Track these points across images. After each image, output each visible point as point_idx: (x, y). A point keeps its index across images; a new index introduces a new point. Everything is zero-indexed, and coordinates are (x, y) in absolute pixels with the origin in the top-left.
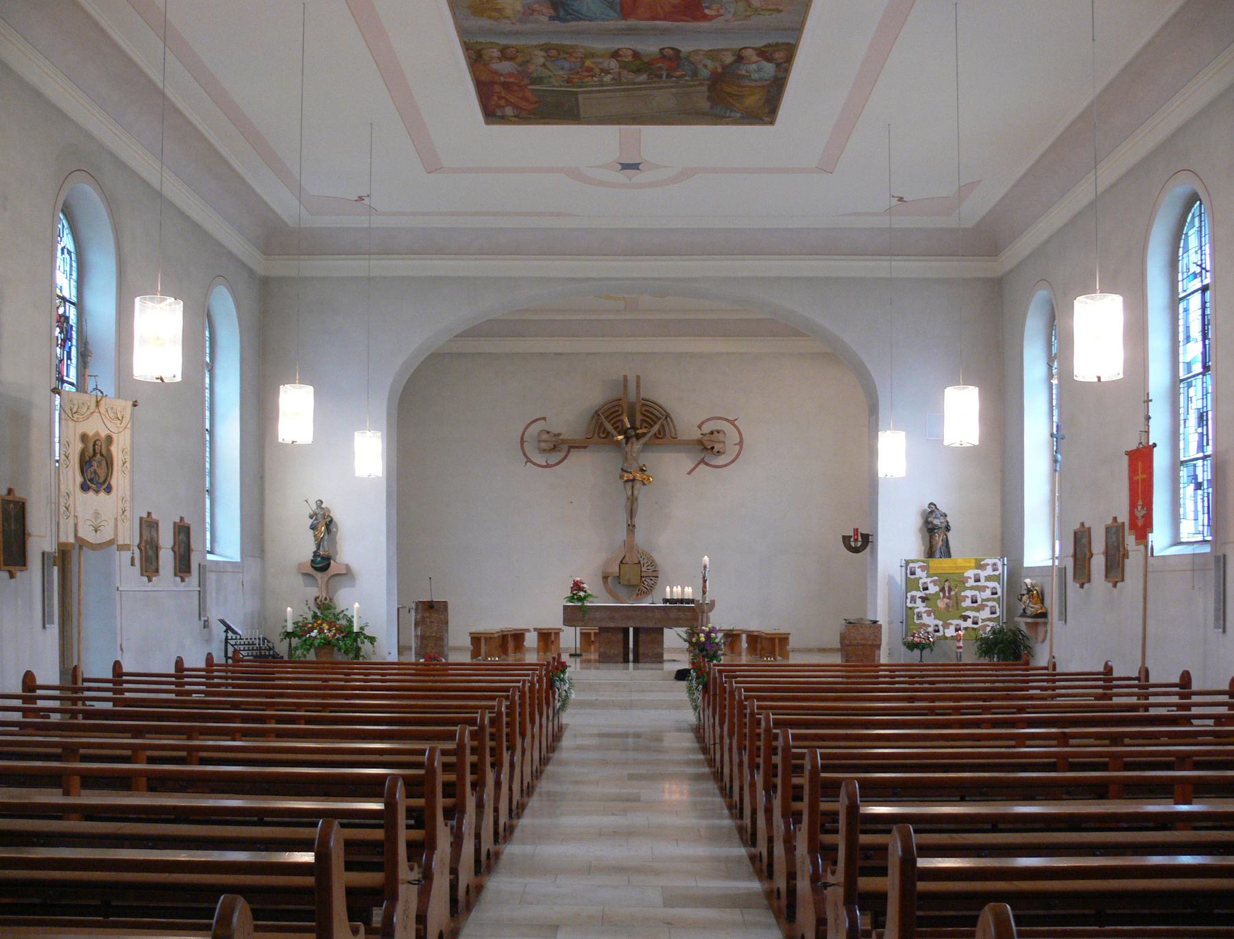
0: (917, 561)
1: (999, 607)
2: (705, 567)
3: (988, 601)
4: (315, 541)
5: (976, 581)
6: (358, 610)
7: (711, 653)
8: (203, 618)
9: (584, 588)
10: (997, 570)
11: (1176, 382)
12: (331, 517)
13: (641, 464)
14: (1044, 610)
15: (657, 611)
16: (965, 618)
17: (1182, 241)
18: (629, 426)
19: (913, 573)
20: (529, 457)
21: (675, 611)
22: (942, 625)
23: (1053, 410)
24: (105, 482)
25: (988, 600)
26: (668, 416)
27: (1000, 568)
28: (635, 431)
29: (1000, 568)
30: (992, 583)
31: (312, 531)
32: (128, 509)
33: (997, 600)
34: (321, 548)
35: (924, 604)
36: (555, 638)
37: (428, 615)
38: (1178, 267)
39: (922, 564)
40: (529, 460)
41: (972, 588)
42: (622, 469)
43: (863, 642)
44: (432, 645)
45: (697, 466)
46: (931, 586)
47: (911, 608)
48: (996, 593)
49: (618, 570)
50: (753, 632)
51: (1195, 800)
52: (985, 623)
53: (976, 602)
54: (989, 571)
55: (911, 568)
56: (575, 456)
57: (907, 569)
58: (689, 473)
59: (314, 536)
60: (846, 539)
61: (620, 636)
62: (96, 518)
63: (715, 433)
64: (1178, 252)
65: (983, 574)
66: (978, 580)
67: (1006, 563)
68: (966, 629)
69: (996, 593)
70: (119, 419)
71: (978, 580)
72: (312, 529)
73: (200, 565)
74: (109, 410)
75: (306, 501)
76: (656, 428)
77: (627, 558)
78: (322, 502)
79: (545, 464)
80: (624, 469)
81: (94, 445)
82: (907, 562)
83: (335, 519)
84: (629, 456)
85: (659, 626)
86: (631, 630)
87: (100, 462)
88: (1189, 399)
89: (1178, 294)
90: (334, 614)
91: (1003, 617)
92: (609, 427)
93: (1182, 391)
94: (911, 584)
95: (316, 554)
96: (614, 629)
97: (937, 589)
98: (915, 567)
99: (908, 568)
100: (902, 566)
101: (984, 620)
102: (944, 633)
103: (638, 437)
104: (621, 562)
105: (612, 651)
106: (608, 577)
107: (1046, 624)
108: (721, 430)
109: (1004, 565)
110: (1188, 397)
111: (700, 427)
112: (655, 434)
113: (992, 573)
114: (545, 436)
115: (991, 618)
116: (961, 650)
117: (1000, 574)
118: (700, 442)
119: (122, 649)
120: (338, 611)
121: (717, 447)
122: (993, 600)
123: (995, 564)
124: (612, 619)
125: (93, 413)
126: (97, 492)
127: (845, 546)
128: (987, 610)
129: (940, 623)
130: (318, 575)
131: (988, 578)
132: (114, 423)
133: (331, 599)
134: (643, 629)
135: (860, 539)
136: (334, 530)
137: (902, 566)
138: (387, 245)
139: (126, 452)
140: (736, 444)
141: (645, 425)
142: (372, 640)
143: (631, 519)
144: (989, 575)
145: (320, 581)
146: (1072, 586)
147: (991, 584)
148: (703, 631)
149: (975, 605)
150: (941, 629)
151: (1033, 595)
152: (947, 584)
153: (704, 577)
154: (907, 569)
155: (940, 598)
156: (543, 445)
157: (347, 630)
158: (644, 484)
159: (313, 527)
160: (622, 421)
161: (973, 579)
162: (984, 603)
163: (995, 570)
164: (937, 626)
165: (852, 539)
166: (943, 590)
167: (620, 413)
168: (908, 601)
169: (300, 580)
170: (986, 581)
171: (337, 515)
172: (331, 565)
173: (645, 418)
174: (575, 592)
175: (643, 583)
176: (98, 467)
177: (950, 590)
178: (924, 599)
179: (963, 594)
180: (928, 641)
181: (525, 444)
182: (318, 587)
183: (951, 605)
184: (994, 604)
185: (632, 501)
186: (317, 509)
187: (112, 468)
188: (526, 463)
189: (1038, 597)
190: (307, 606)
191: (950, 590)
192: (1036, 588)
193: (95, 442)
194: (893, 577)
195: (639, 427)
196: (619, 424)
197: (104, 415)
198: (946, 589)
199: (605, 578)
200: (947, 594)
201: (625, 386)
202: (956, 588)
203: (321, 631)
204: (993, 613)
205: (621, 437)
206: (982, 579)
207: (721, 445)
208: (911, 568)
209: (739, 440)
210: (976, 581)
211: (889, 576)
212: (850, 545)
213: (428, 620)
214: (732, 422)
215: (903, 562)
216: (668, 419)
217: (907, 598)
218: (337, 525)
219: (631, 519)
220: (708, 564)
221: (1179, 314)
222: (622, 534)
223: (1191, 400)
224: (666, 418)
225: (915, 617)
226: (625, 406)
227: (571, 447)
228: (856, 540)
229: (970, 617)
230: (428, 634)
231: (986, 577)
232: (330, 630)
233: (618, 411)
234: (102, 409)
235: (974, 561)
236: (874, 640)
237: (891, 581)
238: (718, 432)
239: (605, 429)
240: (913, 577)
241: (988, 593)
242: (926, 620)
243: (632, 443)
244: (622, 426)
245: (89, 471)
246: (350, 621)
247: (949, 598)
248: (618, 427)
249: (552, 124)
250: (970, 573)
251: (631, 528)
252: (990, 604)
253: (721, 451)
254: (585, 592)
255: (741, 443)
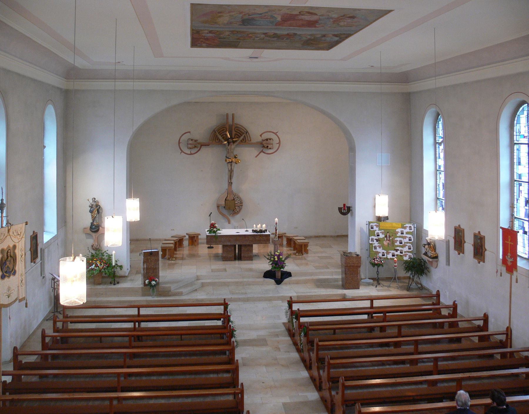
0: (374, 223)
1: (412, 246)
2: (276, 224)
3: (407, 243)
4: (92, 218)
5: (401, 234)
6: (115, 254)
7: (281, 266)
8: (43, 276)
9: (216, 226)
10: (412, 229)
11: (512, 181)
12: (99, 206)
13: (235, 154)
14: (436, 255)
15: (250, 237)
16: (397, 250)
17: (516, 118)
18: (230, 137)
19: (372, 228)
20: (183, 150)
21: (259, 237)
22: (386, 253)
23: (436, 159)
24: (13, 270)
25: (407, 243)
26: (247, 132)
27: (413, 228)
28: (232, 140)
29: (413, 228)
30: (409, 235)
31: (90, 213)
32: (24, 279)
33: (412, 243)
34: (95, 221)
35: (378, 243)
36: (197, 238)
37: (150, 258)
38: (514, 129)
39: (376, 224)
40: (182, 151)
41: (400, 237)
42: (226, 157)
43: (353, 265)
44: (152, 272)
45: (260, 153)
46: (380, 234)
47: (371, 244)
48: (411, 240)
49: (224, 203)
50: (290, 237)
51: (520, 368)
52: (406, 253)
53: (402, 243)
54: (408, 230)
55: (371, 226)
56: (204, 149)
57: (369, 226)
58: (256, 157)
59: (92, 216)
60: (340, 209)
61: (233, 248)
62: (9, 290)
63: (269, 140)
64: (514, 122)
65: (405, 231)
66: (402, 233)
67: (415, 227)
68: (397, 255)
69: (411, 240)
70: (19, 235)
71: (402, 233)
72: (91, 212)
73: (41, 249)
74: (14, 232)
75: (88, 200)
76: (242, 138)
77: (228, 197)
78: (95, 199)
79: (190, 153)
80: (227, 156)
81: (7, 253)
82: (369, 223)
83: (101, 206)
84: (229, 151)
85: (251, 244)
86: (237, 246)
87: (10, 261)
88: (520, 191)
89: (514, 141)
90: (101, 253)
91: (414, 251)
92: (220, 137)
93: (515, 185)
94: (371, 232)
95: (92, 224)
96: (231, 246)
97: (383, 236)
98: (373, 225)
99: (370, 225)
100: (367, 224)
101: (405, 252)
102: (387, 256)
103: (234, 142)
104: (226, 200)
105: (229, 255)
106: (219, 206)
107: (437, 261)
108: (272, 139)
109: (414, 227)
110: (519, 190)
111: (261, 136)
112: (241, 140)
113: (409, 231)
114: (190, 142)
115: (409, 251)
116: (396, 267)
117: (413, 231)
118: (262, 143)
119: (10, 318)
120: (103, 251)
121: (270, 146)
122: (410, 243)
123: (410, 227)
124: (229, 241)
125: (7, 236)
126: (9, 277)
127: (339, 212)
128: (407, 247)
129: (385, 252)
130: (94, 234)
131: (407, 233)
132: (17, 238)
133: (99, 245)
134: (244, 245)
135: (346, 209)
136: (101, 211)
137: (367, 224)
138: (127, 76)
139: (23, 250)
140: (277, 144)
141: (236, 136)
142: (121, 267)
143: (230, 179)
144: (408, 232)
145: (94, 237)
146: (453, 253)
147: (409, 236)
148: (276, 255)
149: (401, 245)
150: (385, 254)
151: (431, 247)
152: (388, 234)
153: (276, 228)
154: (369, 226)
155: (385, 240)
156: (190, 146)
157: (109, 263)
158: (236, 163)
159: (91, 212)
160: (226, 135)
161: (400, 233)
162: (405, 244)
163: (410, 229)
164: (383, 253)
165: (343, 209)
166: (386, 236)
167: (225, 131)
168: (370, 240)
169: (84, 236)
170: (406, 234)
171: (102, 204)
172: (100, 229)
173: (237, 133)
174: (212, 229)
175: (236, 209)
176: (9, 264)
177: (390, 237)
178: (377, 240)
179: (395, 239)
180: (381, 263)
181: (181, 144)
182: (93, 239)
183: (390, 244)
184: (410, 245)
185: (231, 172)
186: (93, 202)
187: (16, 262)
188: (181, 153)
189: (433, 248)
190: (88, 250)
191: (390, 237)
192: (432, 244)
193: (8, 251)
194: (362, 228)
195: (234, 138)
196: (225, 136)
197: (12, 236)
198: (388, 236)
199: (218, 207)
200: (388, 239)
201: (227, 118)
202: (392, 236)
203: (96, 266)
204: (409, 249)
205: (226, 142)
206: (405, 233)
207: (271, 146)
208: (371, 226)
209: (279, 142)
210: (401, 234)
211: (361, 228)
212: (342, 211)
213: (150, 260)
214: (276, 134)
215: (368, 222)
216: (247, 133)
217: (369, 239)
218: (102, 209)
219: (230, 179)
220: (277, 222)
221: (514, 150)
222: (226, 186)
223: (521, 192)
224: (246, 133)
225: (373, 248)
226: (228, 127)
227: (201, 146)
228: (344, 209)
229: (399, 250)
230: (149, 267)
231: (406, 232)
232: (101, 264)
233: (224, 130)
234: (11, 233)
235: (401, 224)
236: (358, 264)
237: (361, 230)
238: (270, 140)
239: (218, 138)
240: (372, 230)
241: (407, 240)
242: (379, 250)
243: (231, 145)
244: (226, 136)
245: (5, 268)
246: (110, 256)
247: (389, 240)
248: (224, 137)
249: (221, 48)
250: (399, 230)
251: (230, 184)
252: (408, 245)
253: (271, 148)
254: (217, 228)
255: (279, 143)
